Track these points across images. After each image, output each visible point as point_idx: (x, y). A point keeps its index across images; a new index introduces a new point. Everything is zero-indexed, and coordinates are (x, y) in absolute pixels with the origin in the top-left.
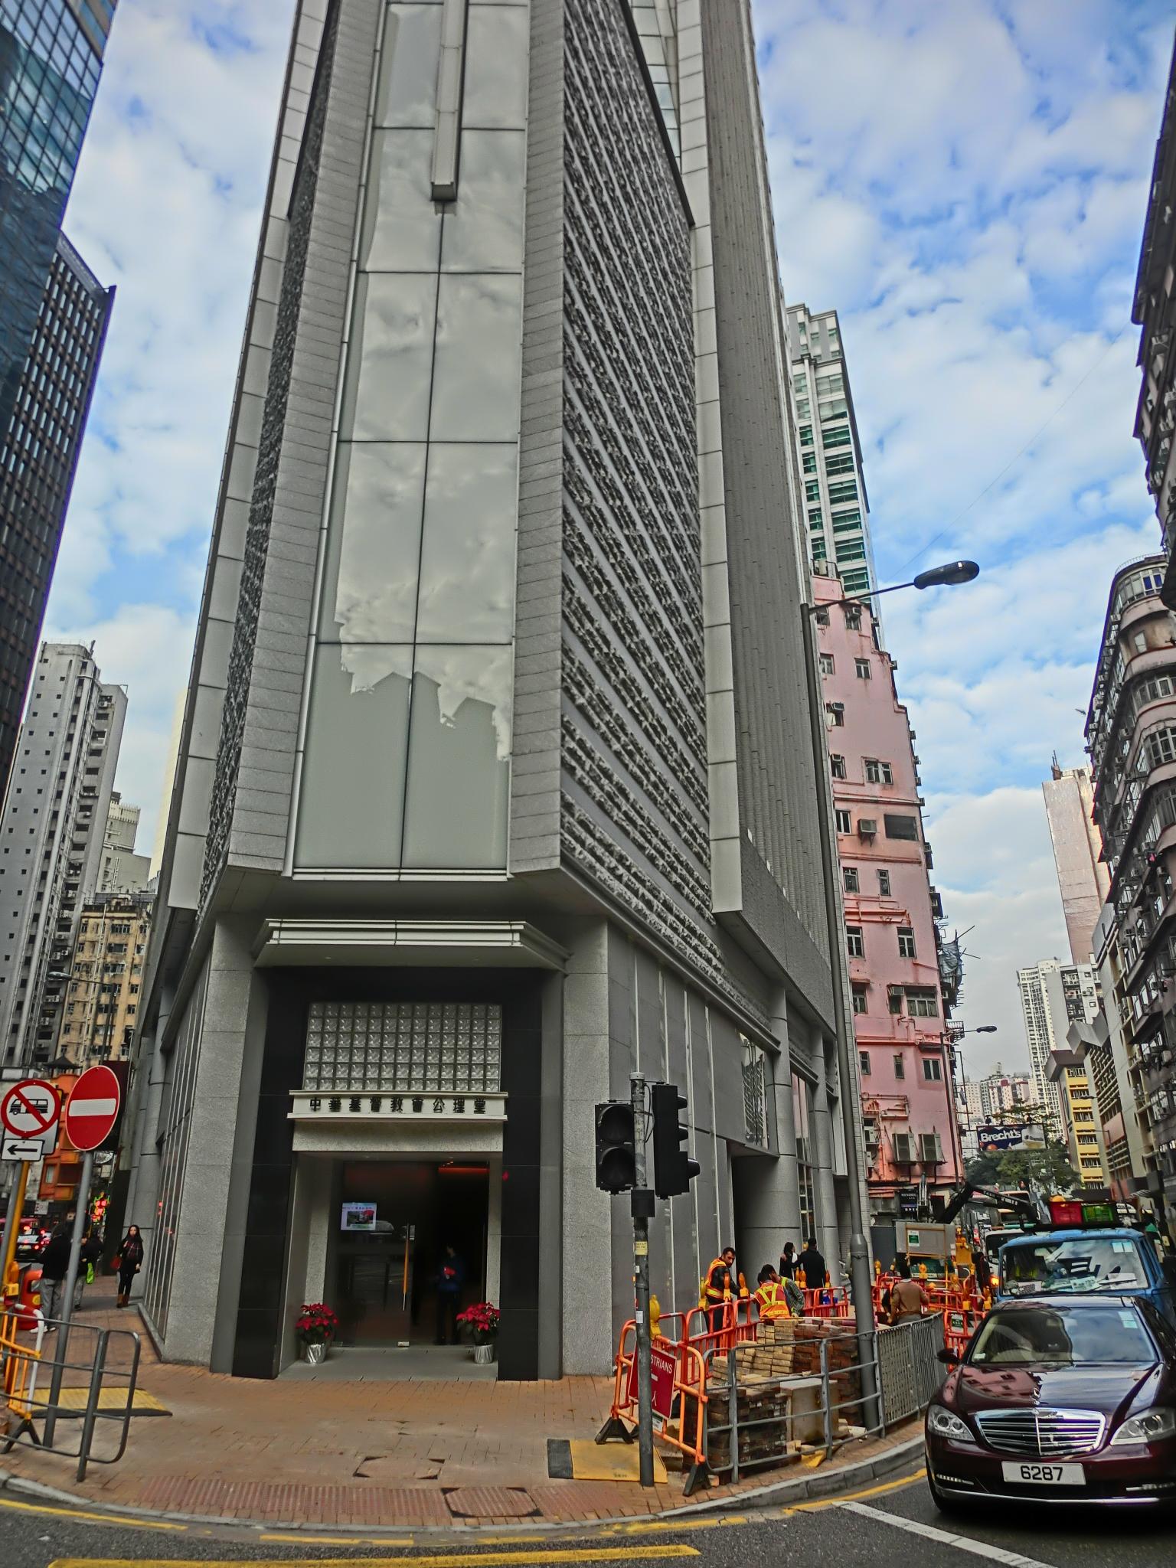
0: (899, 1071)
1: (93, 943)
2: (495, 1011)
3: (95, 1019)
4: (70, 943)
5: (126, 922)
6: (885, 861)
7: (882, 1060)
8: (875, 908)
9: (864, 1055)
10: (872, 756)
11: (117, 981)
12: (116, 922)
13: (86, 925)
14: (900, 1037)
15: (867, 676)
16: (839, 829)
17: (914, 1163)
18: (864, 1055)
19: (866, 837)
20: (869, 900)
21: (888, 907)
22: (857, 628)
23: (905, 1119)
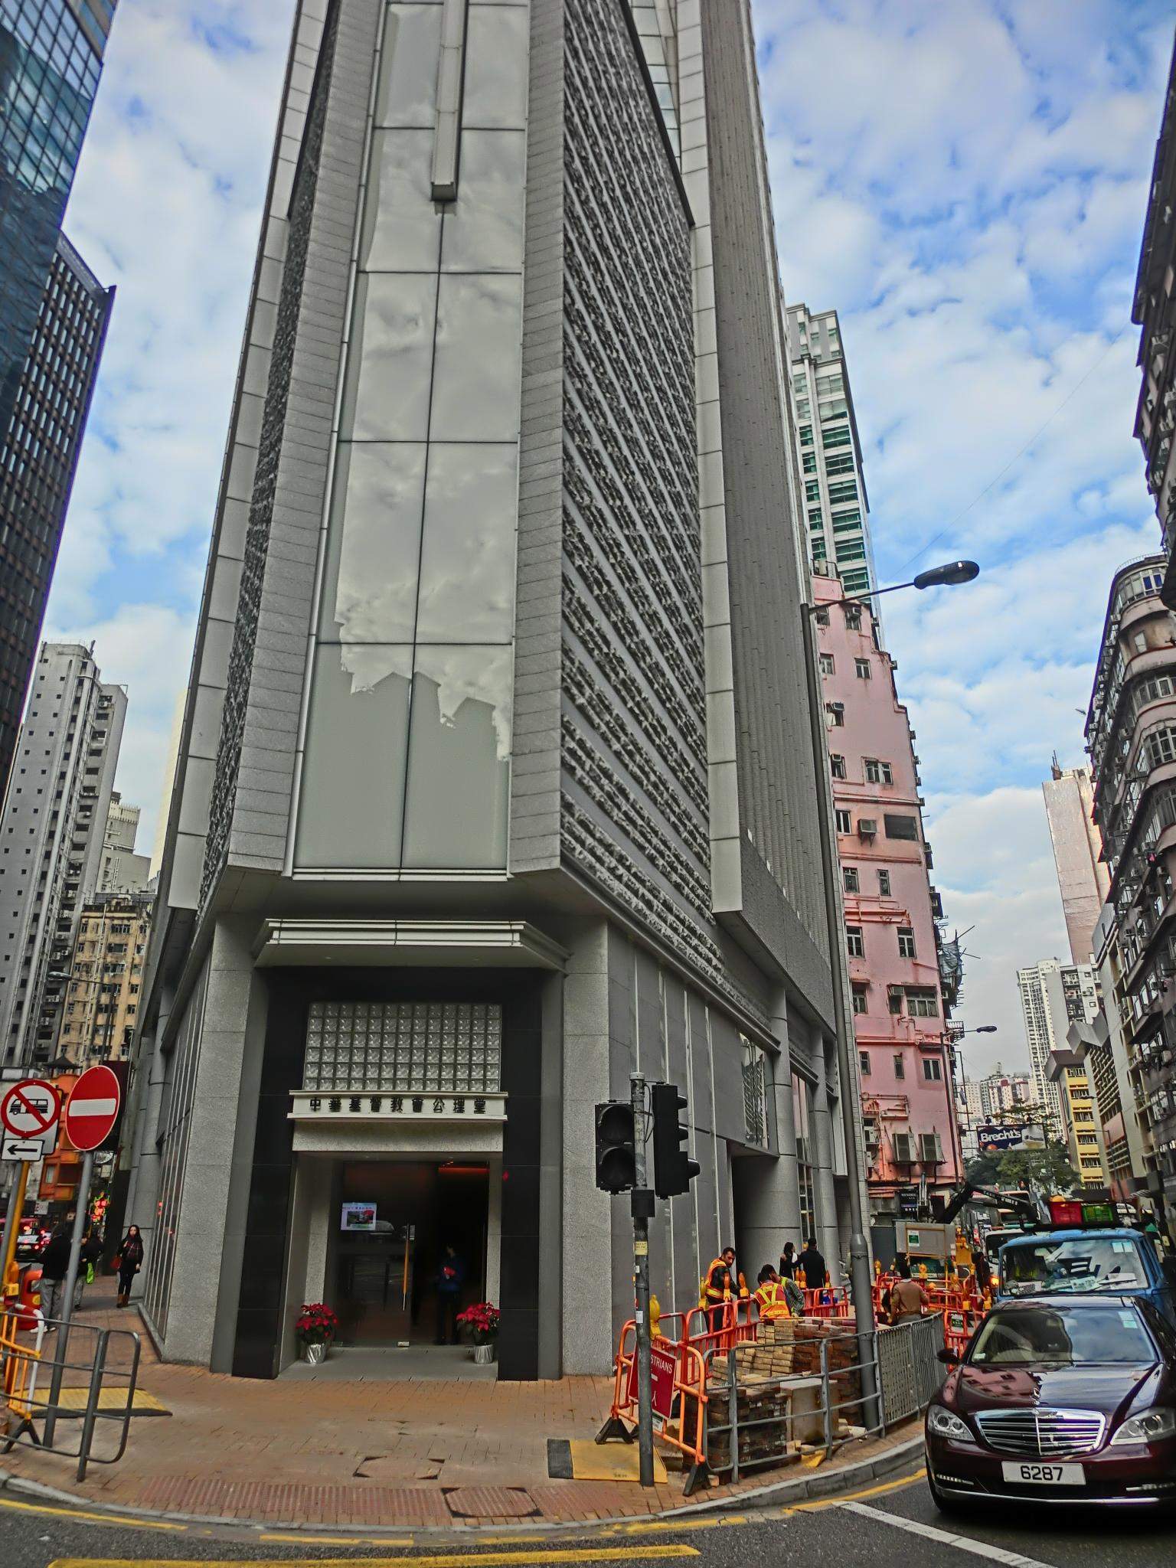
0: (899, 1071)
1: (93, 943)
3: (95, 1019)
4: (70, 943)
5: (126, 922)
6: (885, 861)
7: (882, 1060)
8: (875, 908)
9: (864, 1055)
10: (872, 756)
11: (117, 981)
12: (116, 922)
13: (86, 925)
14: (900, 1037)
15: (867, 676)
16: (839, 829)
17: (914, 1163)
18: (864, 1055)
19: (866, 837)
20: (869, 900)
21: (888, 907)
22: (857, 628)
23: (905, 1119)
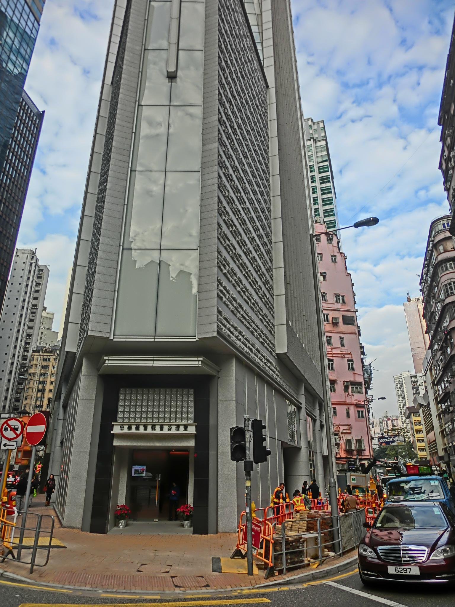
0: (348, 414)
1: (36, 365)
2: (192, 391)
3: (37, 395)
4: (27, 365)
5: (49, 357)
6: (342, 333)
7: (341, 410)
8: (338, 351)
10: (338, 292)
11: (45, 380)
12: (45, 357)
13: (33, 358)
14: (348, 401)
15: (336, 262)
16: (325, 321)
17: (354, 450)
19: (335, 324)
20: (336, 348)
21: (344, 351)
23: (350, 433)
